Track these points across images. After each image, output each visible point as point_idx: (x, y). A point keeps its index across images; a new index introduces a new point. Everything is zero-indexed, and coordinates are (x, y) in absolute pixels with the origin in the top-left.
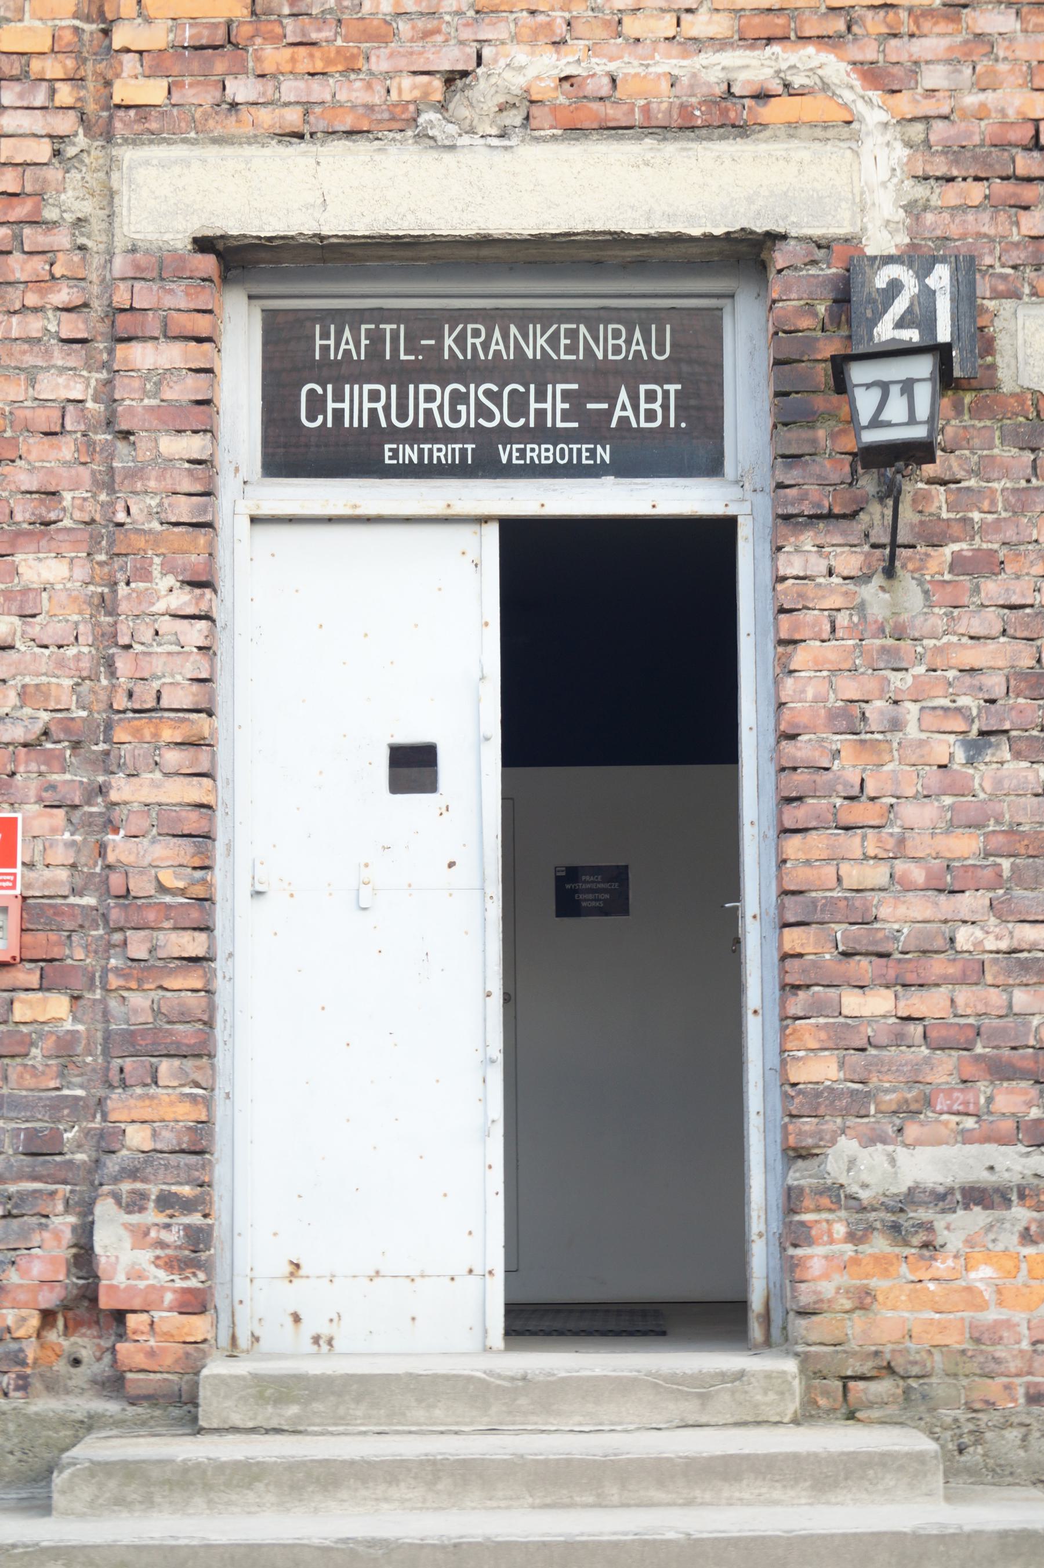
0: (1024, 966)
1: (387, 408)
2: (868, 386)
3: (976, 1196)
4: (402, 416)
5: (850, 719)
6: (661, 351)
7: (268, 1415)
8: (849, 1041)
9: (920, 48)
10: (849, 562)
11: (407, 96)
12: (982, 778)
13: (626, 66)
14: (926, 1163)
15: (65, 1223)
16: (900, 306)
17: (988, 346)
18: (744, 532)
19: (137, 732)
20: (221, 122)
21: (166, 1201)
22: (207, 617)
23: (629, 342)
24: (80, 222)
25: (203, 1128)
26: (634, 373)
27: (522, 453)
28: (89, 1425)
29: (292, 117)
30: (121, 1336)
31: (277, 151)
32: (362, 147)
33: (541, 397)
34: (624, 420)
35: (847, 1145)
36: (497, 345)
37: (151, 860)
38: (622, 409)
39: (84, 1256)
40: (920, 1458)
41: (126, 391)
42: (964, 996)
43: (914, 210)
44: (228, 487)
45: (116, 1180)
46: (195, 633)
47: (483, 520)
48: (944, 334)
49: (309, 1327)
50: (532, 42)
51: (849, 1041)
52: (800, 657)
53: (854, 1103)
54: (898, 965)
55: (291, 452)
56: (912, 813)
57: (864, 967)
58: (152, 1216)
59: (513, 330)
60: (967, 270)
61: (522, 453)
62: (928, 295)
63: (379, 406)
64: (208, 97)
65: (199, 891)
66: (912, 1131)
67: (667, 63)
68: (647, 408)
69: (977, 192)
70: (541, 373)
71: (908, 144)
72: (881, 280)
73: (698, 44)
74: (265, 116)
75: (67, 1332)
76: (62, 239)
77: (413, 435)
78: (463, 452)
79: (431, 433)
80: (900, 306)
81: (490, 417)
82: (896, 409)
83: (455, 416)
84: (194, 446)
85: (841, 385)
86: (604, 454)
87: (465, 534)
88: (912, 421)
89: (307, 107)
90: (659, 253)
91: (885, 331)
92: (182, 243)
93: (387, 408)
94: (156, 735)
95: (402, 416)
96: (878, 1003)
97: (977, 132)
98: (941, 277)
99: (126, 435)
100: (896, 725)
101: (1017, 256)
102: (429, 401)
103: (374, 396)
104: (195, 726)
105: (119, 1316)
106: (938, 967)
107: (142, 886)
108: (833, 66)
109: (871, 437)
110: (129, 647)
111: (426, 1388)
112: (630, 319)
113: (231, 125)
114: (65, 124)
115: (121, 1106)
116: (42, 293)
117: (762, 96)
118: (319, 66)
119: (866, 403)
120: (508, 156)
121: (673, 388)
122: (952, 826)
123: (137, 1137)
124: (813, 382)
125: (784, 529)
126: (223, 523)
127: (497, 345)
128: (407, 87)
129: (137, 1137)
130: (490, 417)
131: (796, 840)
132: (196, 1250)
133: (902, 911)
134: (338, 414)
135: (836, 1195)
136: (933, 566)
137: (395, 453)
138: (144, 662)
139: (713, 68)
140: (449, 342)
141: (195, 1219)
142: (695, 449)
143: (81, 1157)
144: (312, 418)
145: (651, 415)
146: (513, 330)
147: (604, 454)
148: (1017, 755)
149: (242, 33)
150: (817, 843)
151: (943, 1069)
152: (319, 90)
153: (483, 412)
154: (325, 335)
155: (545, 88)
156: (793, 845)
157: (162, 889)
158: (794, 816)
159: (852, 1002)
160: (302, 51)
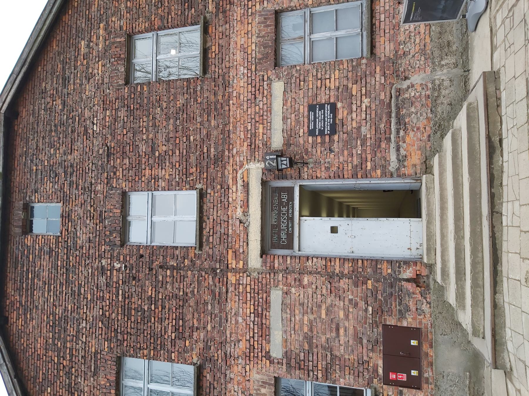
0: (364, 144)
3: (398, 150)
5: (327, 169)
8: (374, 168)
9: (238, 161)
10: (306, 169)
12: (336, 150)
13: (239, 199)
14: (393, 157)
15: (403, 283)
16: (271, 163)
17: (277, 151)
20: (246, 253)
21: (399, 267)
22: (312, 258)
24: (258, 273)
25: (388, 261)
26: (280, 199)
28: (435, 281)
29: (245, 243)
30: (420, 275)
31: (249, 246)
32: (249, 234)
35: (390, 168)
37: (347, 267)
38: (285, 200)
39: (408, 280)
40: (439, 157)
42: (368, 152)
43: (258, 161)
44: (294, 254)
45: (396, 275)
46: (315, 260)
47: (299, 219)
48: (275, 157)
49: (419, 247)
51: (374, 168)
52: (319, 176)
53: (384, 167)
54: (363, 161)
55: (290, 246)
56: (341, 160)
58: (401, 269)
60: (267, 154)
64: (242, 255)
65: (352, 261)
66: (388, 159)
68: (285, 197)
69: (257, 153)
70: (280, 211)
73: (237, 190)
74: (245, 247)
75: (420, 283)
76: (260, 276)
77: (288, 229)
79: (287, 226)
80: (271, 163)
84: (289, 258)
85: (281, 170)
86: (291, 203)
87: (302, 222)
88: (286, 160)
89: (244, 242)
90: (264, 195)
91: (275, 164)
92: (261, 259)
96: (369, 164)
97: (249, 153)
98: (268, 158)
99: (287, 268)
101: (265, 147)
102: (283, 226)
104: (328, 259)
105: (417, 275)
106: (364, 156)
107: (351, 269)
108: (240, 172)
109: (288, 166)
111: (430, 237)
113: (246, 252)
114: (245, 275)
115: (384, 274)
117: (244, 181)
119: (284, 166)
123: (389, 271)
124: (281, 174)
126: (299, 255)
128: (241, 228)
129: (389, 271)
131: (345, 176)
132: (407, 263)
133: (355, 161)
135: (398, 169)
136: (306, 158)
139: (240, 188)
141: (402, 263)
142: (290, 191)
145: (286, 196)
147: (291, 203)
148: (333, 145)
149: (234, 250)
151: (379, 155)
152: (242, 240)
155: (242, 210)
156: (346, 176)
157: (352, 266)
158: (341, 176)
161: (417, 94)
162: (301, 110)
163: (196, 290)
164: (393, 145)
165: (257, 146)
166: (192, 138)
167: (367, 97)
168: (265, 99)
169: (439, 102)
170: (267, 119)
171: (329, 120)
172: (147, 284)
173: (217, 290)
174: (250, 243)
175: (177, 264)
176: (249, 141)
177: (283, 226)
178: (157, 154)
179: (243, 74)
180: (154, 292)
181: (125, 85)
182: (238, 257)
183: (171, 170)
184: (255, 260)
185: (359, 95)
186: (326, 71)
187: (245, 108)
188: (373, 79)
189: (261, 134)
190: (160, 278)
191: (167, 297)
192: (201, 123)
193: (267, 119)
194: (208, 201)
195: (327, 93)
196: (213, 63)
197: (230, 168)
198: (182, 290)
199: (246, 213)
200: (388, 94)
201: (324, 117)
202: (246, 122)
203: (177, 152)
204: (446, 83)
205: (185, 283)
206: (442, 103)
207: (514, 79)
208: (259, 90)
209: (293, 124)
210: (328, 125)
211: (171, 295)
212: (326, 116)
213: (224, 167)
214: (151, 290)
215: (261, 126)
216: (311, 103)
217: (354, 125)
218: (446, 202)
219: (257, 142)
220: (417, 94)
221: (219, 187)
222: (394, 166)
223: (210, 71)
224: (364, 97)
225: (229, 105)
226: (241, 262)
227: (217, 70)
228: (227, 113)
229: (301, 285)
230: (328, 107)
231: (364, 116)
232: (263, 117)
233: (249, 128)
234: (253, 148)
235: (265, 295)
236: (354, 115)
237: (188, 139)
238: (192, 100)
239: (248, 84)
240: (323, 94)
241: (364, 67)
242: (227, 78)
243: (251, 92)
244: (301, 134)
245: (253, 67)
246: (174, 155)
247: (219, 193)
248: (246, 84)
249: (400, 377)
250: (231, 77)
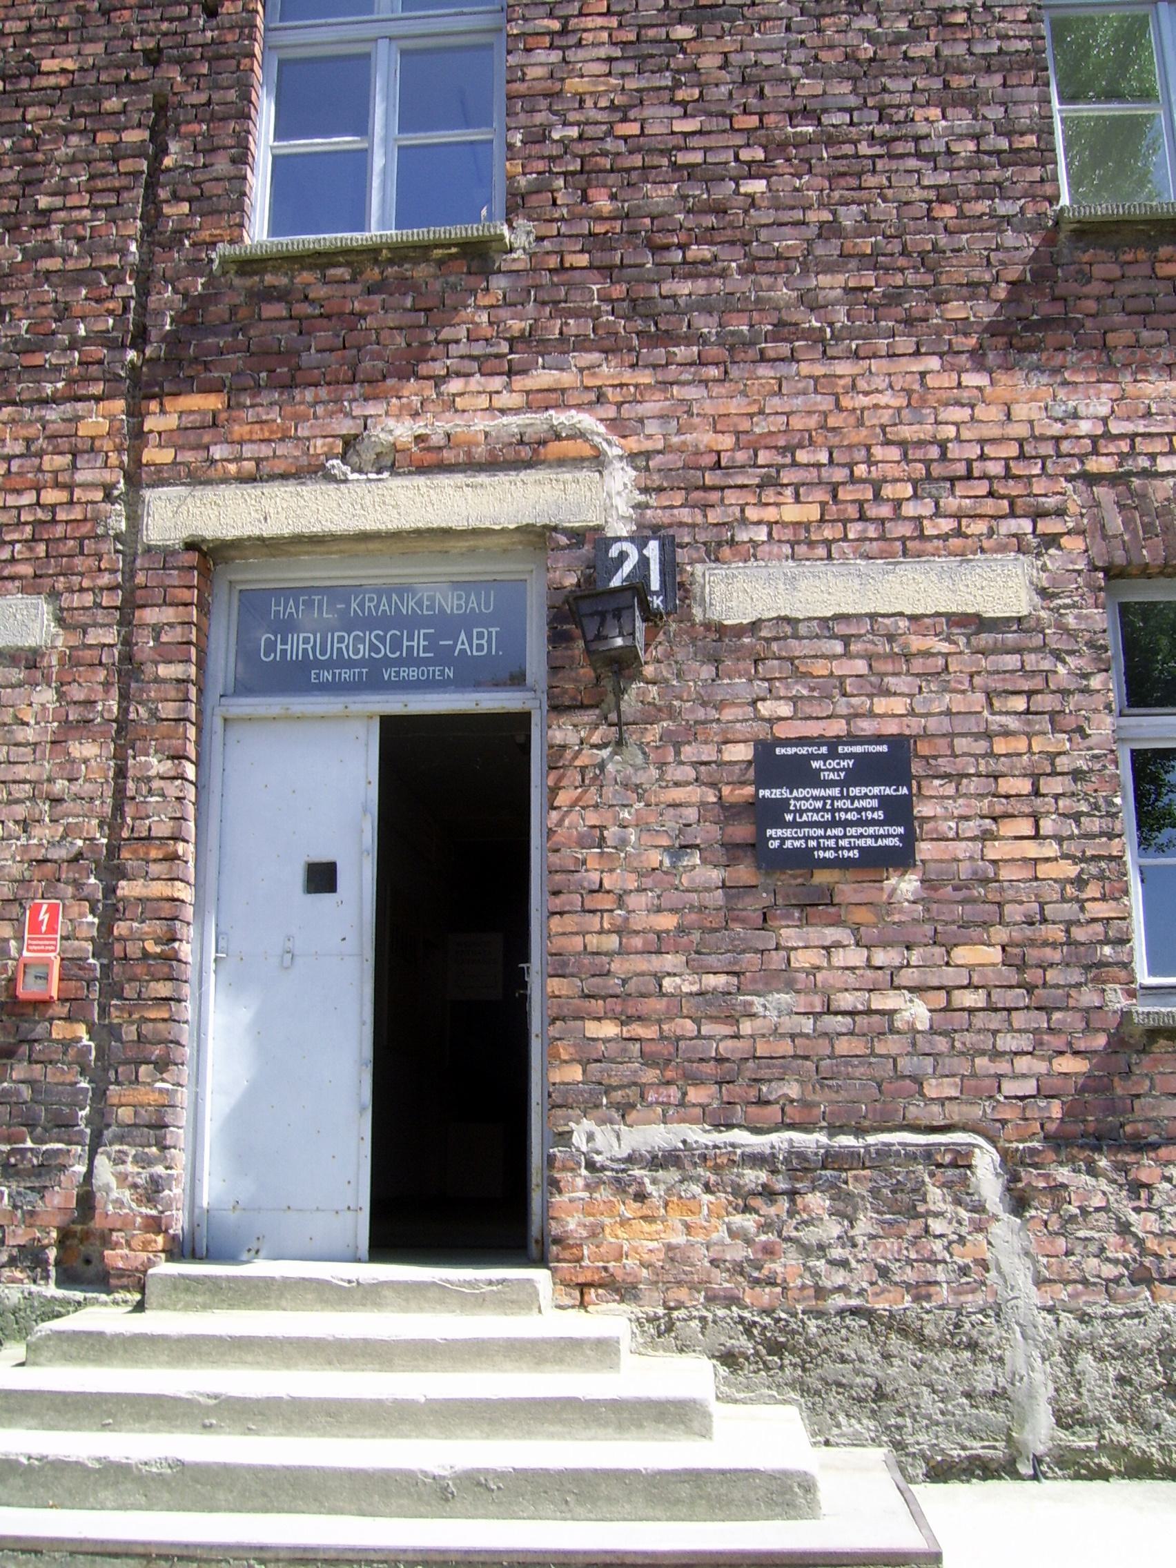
1: (314, 648)
2: (592, 615)
4: (323, 653)
6: (487, 607)
9: (641, 410)
11: (319, 451)
18: (535, 719)
19: (135, 852)
20: (197, 478)
23: (467, 603)
27: (398, 673)
29: (249, 466)
33: (411, 638)
34: (463, 651)
36: (384, 606)
38: (462, 643)
50: (398, 417)
57: (598, 1006)
58: (130, 1168)
59: (394, 597)
60: (669, 547)
61: (398, 673)
62: (644, 562)
63: (309, 647)
71: (635, 468)
72: (614, 552)
77: (329, 665)
78: (360, 674)
80: (627, 567)
81: (378, 651)
83: (356, 652)
86: (450, 673)
89: (258, 461)
93: (314, 648)
94: (147, 853)
95: (323, 653)
96: (609, 1029)
98: (653, 550)
100: (624, 842)
103: (306, 641)
106: (754, 1177)
107: (133, 950)
108: (586, 420)
110: (133, 798)
116: (93, 579)
118: (267, 435)
120: (380, 485)
121: (494, 630)
122: (659, 910)
125: (553, 715)
127: (384, 606)
130: (378, 651)
134: (284, 652)
136: (649, 737)
137: (318, 675)
138: (141, 807)
140: (354, 605)
143: (111, 321)
144: (267, 655)
146: (394, 597)
150: (569, 923)
152: (265, 451)
153: (374, 649)
154: (278, 604)
159: (594, 1029)
160: (257, 427)
161: (937, 1246)
162: (881, 704)
163: (53, 264)
164: (700, 1136)
165: (714, 496)
166: (758, 186)
167: (936, 1016)
168: (946, 525)
169: (895, 1340)
170: (845, 539)
171: (832, 843)
172: (89, 49)
173: (51, 358)
174: (252, 491)
175: (168, 170)
176: (741, 457)
177: (341, 640)
178: (683, 32)
179: (1075, 416)
180: (52, 81)
181: (1046, 1138)
182: (192, 437)
183: (603, 103)
184: (173, 516)
185: (950, 976)
186: (1077, 817)
187: (906, 432)
188: (1024, 1042)
189: (770, 514)
190: (113, 104)
191: (28, 143)
192: (830, 230)
193: (845, 539)
194: (452, 279)
195: (964, 825)
196: (1131, 271)
197: (609, 372)
198: (58, 201)
199: (393, 462)
200: (956, 1113)
201: (846, 824)
202: (835, 440)
203: (691, 125)
204: (985, 1377)
205: (86, 213)
206: (887, 1356)
207: (1025, 626)
208: (991, 494)
209: (820, 667)
210: (807, 838)
211: (40, 157)
212: (852, 831)
213: (610, 346)
214: (64, 71)
215: (813, 513)
216: (923, 748)
217: (802, 959)
218: (566, 1512)
219: (732, 497)
220: (937, 1246)
221: (517, 326)
222: (600, 1142)
223: (1086, 258)
224: (940, 999)
225: (917, 353)
226: (166, 456)
227: (1095, 288)
228: (882, 343)
229: (71, 728)
230: (891, 837)
231: (846, 1001)
232: (859, 522)
233: (802, 456)
234: (697, 478)
235: (26, 569)
236: (856, 957)
237: (753, 170)
238: (945, 178)
239: (1021, 442)
240: (960, 807)
241: (1088, 997)
242: (1053, 337)
243: (983, 457)
244: (765, 709)
245: (1103, 464)
246: (678, 111)
247: (488, 332)
248: (1022, 431)
249: (44, 916)
250: (1059, 359)
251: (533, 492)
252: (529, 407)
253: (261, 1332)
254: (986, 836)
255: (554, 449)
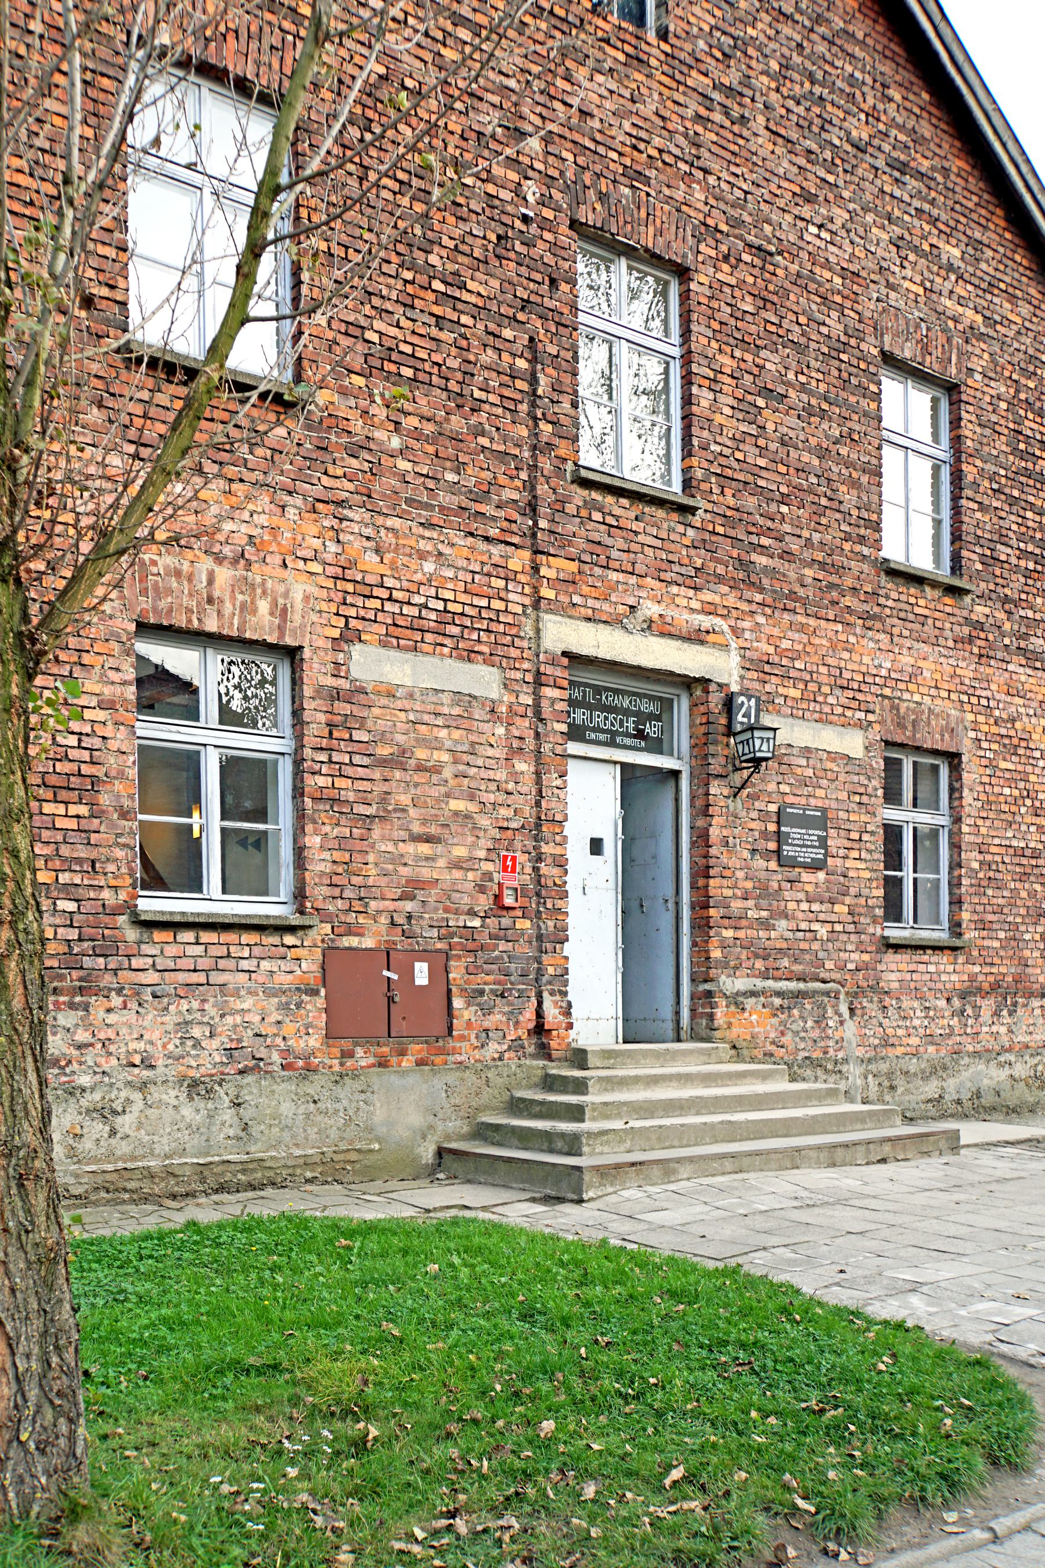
3: (753, 994)
7: (606, 1063)
39: (539, 1014)
41: (544, 703)
43: (742, 677)
47: (615, 763)
57: (726, 922)
67: (686, 616)
82: (765, 747)
87: (611, 767)
106: (744, 922)
112: (651, 698)
113: (572, 612)
128: (621, 609)
152: (597, 605)
164: (760, 984)
180: (473, 299)
184: (563, 634)
185: (834, 918)
217: (792, 905)
236: (804, 906)
247: (686, 561)
251: (916, 1172)
252: (703, 612)
253: (604, 653)
254: (846, 857)
255: (711, 638)
